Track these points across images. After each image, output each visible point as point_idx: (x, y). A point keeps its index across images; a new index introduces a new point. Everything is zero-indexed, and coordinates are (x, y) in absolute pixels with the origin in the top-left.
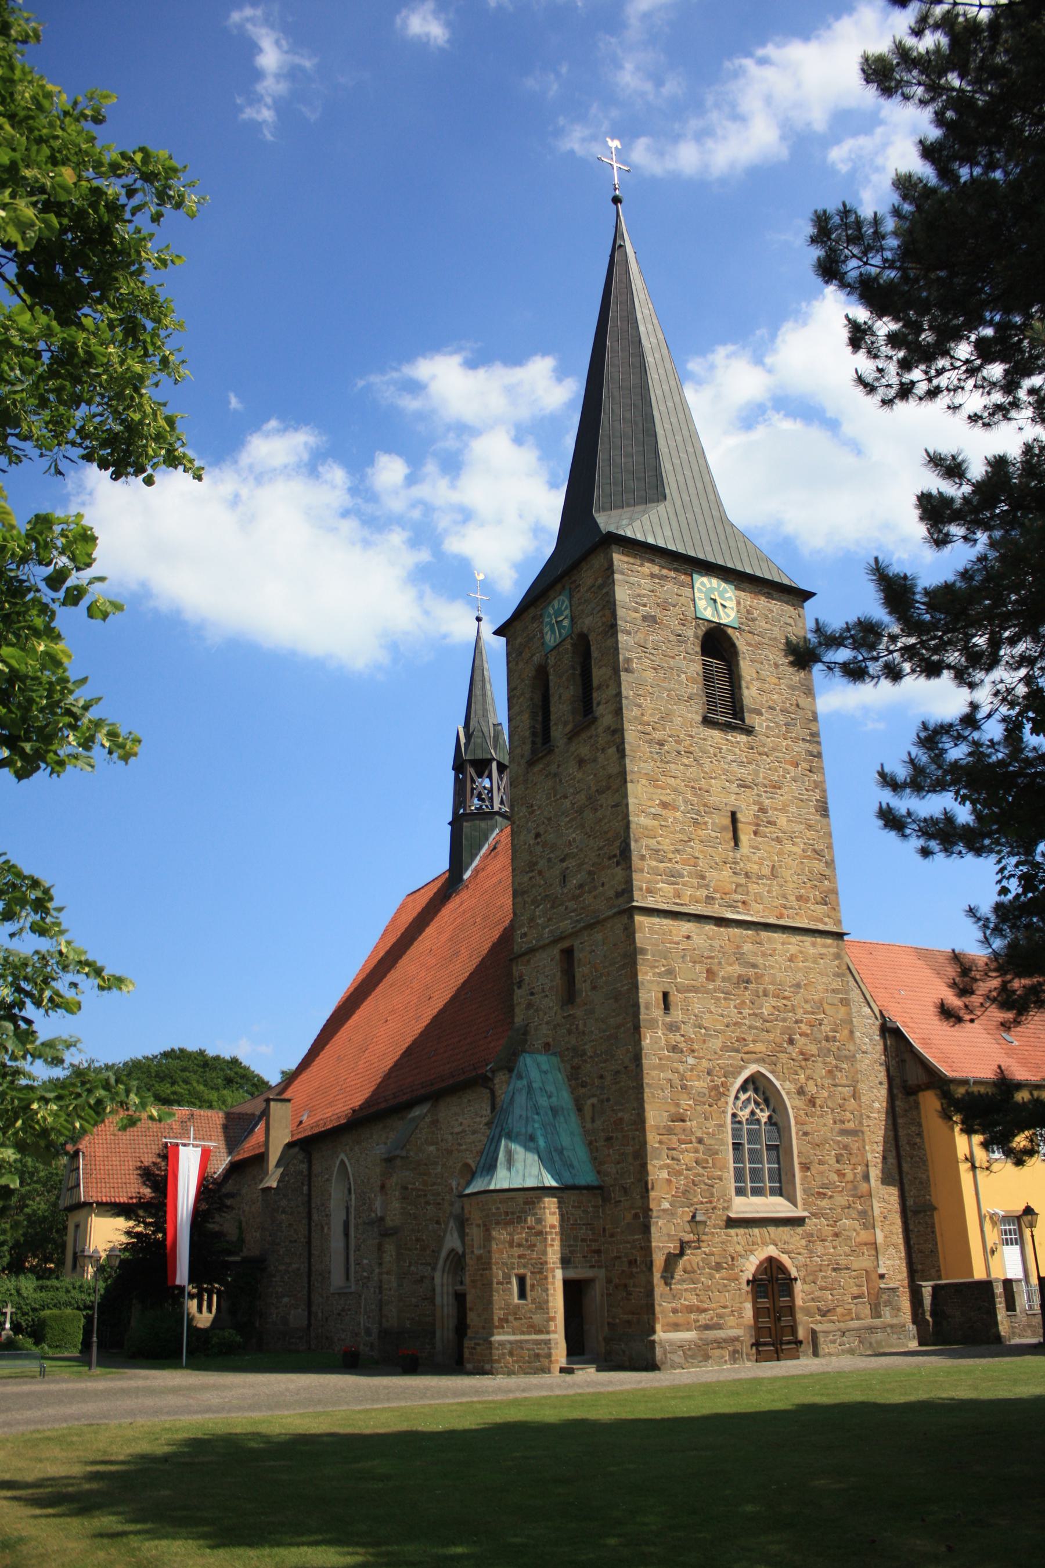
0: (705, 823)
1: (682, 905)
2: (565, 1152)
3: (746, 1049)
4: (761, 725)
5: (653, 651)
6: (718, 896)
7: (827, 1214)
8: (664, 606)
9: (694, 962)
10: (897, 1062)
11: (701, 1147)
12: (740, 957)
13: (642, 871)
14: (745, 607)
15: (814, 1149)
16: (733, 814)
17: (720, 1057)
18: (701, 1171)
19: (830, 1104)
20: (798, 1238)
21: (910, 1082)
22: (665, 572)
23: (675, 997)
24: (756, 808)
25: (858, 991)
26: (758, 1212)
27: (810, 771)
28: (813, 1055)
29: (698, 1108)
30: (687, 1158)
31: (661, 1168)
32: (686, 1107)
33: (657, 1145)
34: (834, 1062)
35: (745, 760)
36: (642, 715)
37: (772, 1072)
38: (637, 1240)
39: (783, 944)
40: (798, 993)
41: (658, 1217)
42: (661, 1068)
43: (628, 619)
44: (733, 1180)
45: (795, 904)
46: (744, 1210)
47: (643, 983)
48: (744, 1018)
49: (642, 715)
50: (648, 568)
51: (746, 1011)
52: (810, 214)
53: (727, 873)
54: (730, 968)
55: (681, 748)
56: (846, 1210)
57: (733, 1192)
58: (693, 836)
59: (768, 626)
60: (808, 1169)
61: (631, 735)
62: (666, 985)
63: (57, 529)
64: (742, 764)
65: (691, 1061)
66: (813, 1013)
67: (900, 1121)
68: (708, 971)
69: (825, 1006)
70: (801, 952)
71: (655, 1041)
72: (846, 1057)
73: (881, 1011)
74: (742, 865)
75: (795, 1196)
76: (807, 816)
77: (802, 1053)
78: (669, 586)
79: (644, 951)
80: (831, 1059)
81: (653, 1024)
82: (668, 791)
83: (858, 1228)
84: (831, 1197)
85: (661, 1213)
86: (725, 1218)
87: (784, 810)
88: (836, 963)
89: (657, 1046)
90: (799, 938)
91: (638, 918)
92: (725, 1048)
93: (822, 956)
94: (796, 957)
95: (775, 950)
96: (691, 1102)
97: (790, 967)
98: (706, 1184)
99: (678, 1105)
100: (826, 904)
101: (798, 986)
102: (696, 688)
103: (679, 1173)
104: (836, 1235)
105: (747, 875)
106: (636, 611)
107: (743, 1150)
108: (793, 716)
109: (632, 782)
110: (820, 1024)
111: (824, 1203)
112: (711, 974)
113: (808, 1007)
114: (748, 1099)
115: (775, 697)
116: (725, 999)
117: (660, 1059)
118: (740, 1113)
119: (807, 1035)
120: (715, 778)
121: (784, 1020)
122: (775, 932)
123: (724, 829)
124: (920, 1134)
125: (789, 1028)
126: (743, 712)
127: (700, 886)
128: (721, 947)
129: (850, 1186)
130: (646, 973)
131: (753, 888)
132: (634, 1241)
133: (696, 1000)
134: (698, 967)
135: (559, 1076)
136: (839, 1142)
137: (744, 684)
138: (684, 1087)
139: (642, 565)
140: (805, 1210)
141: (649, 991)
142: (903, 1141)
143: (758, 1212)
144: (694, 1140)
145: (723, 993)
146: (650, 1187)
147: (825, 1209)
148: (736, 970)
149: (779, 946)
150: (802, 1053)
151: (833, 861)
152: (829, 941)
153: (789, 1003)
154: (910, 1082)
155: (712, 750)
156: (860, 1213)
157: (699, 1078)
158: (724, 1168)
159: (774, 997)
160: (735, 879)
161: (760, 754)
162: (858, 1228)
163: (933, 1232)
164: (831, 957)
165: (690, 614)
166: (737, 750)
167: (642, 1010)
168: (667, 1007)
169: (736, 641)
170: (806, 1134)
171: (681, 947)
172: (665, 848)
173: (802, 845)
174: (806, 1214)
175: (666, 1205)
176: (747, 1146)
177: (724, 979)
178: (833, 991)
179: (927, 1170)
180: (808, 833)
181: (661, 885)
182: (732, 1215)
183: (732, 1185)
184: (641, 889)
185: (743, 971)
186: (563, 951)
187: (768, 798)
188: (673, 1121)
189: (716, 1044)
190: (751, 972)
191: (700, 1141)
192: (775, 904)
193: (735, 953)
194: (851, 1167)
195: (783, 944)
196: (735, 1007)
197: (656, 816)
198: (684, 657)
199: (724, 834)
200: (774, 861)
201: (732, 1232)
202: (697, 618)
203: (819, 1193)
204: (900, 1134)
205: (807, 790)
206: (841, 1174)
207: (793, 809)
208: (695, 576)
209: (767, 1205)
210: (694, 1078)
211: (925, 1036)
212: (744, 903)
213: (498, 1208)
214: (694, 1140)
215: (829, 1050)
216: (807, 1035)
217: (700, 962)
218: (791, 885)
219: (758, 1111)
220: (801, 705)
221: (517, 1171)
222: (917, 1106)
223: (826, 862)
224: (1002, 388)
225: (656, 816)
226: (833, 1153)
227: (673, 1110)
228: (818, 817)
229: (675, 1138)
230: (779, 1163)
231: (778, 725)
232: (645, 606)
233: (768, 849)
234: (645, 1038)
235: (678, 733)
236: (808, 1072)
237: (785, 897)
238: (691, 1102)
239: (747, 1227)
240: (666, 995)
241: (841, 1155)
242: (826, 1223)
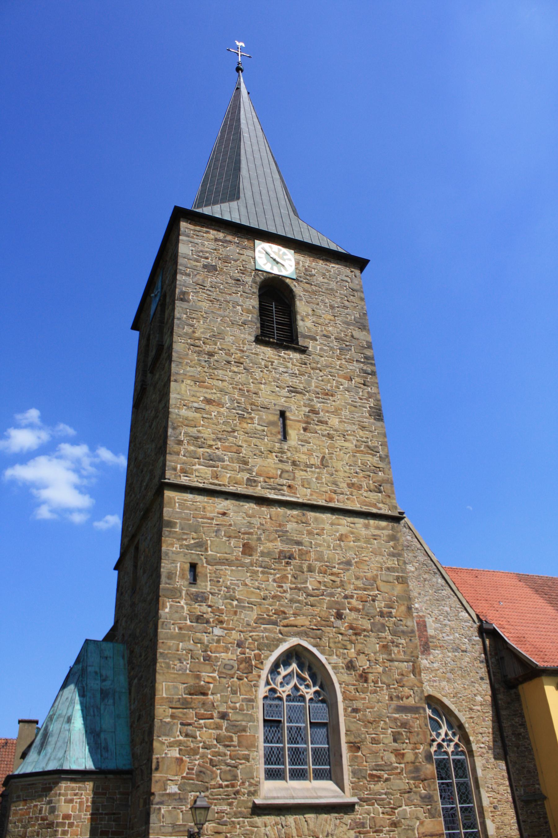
0: (252, 419)
1: (220, 485)
2: (102, 736)
3: (285, 622)
4: (315, 348)
5: (210, 289)
6: (261, 479)
7: (383, 800)
8: (226, 260)
9: (229, 537)
10: (497, 660)
11: (225, 724)
12: (283, 535)
13: (178, 454)
14: (303, 266)
15: (365, 726)
16: (283, 414)
17: (254, 630)
18: (222, 749)
19: (385, 679)
20: (345, 828)
21: (509, 677)
22: (229, 238)
23: (205, 569)
24: (307, 409)
25: (455, 598)
26: (293, 798)
27: (364, 385)
28: (364, 630)
29: (224, 681)
30: (205, 735)
31: (171, 745)
32: (207, 680)
33: (168, 720)
34: (390, 637)
35: (297, 372)
36: (194, 332)
37: (315, 646)
39: (332, 524)
40: (348, 570)
41: (162, 803)
42: (181, 638)
43: (189, 266)
44: (262, 760)
45: (346, 490)
46: (275, 795)
47: (167, 554)
48: (285, 592)
49: (194, 332)
50: (213, 233)
51: (287, 586)
53: (272, 461)
54: (270, 545)
55: (231, 359)
56: (406, 795)
57: (262, 775)
58: (238, 428)
59: (326, 281)
60: (359, 748)
61: (179, 346)
62: (194, 556)
63: (497, 657)
64: (294, 375)
65: (217, 631)
66: (365, 590)
67: (503, 713)
68: (244, 545)
69: (379, 582)
70: (352, 533)
71: (177, 610)
72: (403, 632)
73: (478, 616)
74: (289, 454)
75: (342, 779)
76: (361, 419)
77: (351, 628)
78: (231, 248)
79: (171, 524)
80: (387, 635)
81: (175, 594)
82: (214, 391)
83: (422, 816)
84: (387, 780)
85: (165, 798)
86: (250, 804)
87: (336, 412)
88: (392, 543)
89: (177, 615)
90: (350, 519)
91: (168, 494)
92: (260, 620)
93: (375, 537)
94: (346, 537)
95: (323, 529)
96: (215, 675)
97: (340, 546)
98: (228, 765)
99: (198, 677)
100: (380, 492)
101: (348, 563)
102: (253, 317)
103: (195, 752)
104: (394, 824)
105: (294, 463)
106: (197, 261)
107: (283, 729)
108: (348, 343)
109: (176, 381)
110: (374, 600)
111: (379, 787)
112: (248, 549)
113: (359, 583)
114: (290, 675)
115: (330, 329)
116: (263, 573)
117: (180, 629)
118: (280, 689)
119: (358, 610)
120: (265, 384)
121: (332, 595)
122: (323, 513)
123: (271, 424)
124: (523, 725)
125: (337, 603)
126: (297, 337)
127: (241, 470)
128: (261, 524)
129: (410, 767)
130: (172, 545)
131: (299, 474)
133: (229, 572)
134: (233, 542)
135: (121, 662)
136: (396, 719)
137: (299, 317)
138: (207, 659)
139: (207, 232)
140: (354, 795)
141: (174, 562)
142: (508, 732)
143: (293, 798)
144: (215, 715)
145: (261, 567)
146: (154, 766)
147: (381, 794)
148: (279, 546)
149: (327, 527)
150: (351, 628)
151: (387, 456)
152: (383, 524)
153: (338, 580)
154: (509, 677)
155: (263, 363)
156: (423, 798)
157: (226, 650)
158: (252, 746)
159: (320, 572)
160: (281, 466)
161: (312, 369)
162: (422, 816)
163: (547, 823)
164: (385, 538)
165: (250, 266)
166: (290, 365)
167: (163, 579)
168: (194, 581)
169: (293, 288)
170: (356, 710)
171: (214, 522)
172: (205, 436)
173: (355, 442)
174: (355, 800)
175: (173, 789)
176: (286, 724)
177: (263, 554)
178: (388, 569)
179: (533, 759)
180: (361, 433)
181: (197, 467)
182: (258, 801)
183: (261, 767)
184: (175, 469)
185: (286, 548)
187: (320, 403)
188: (191, 694)
189: (252, 616)
190: (295, 549)
191: (224, 716)
192: (324, 489)
193: (277, 531)
194: (411, 746)
195: (332, 524)
196: (274, 581)
197: (197, 409)
198: (241, 295)
199: (271, 427)
200: (325, 453)
201: (258, 820)
202: (256, 270)
203: (371, 776)
204: (504, 725)
205: (361, 399)
206: (400, 755)
207: (345, 413)
208: (257, 242)
209: (308, 790)
210: (221, 650)
211: (520, 635)
212: (289, 486)
214: (215, 715)
215: (383, 625)
216: (358, 610)
217: (236, 537)
218: (341, 474)
219: (302, 687)
220: (355, 336)
221: (46, 755)
222: (518, 698)
223: (380, 457)
225: (197, 409)
226: (389, 731)
227: (192, 682)
228: (372, 421)
229: (192, 713)
230: (328, 744)
231: (332, 349)
232: (207, 258)
233: (317, 442)
234: (164, 607)
235: (229, 348)
236: (359, 646)
237: (335, 483)
238: (215, 675)
239: (278, 815)
240: (193, 567)
241: (399, 733)
242: (381, 810)
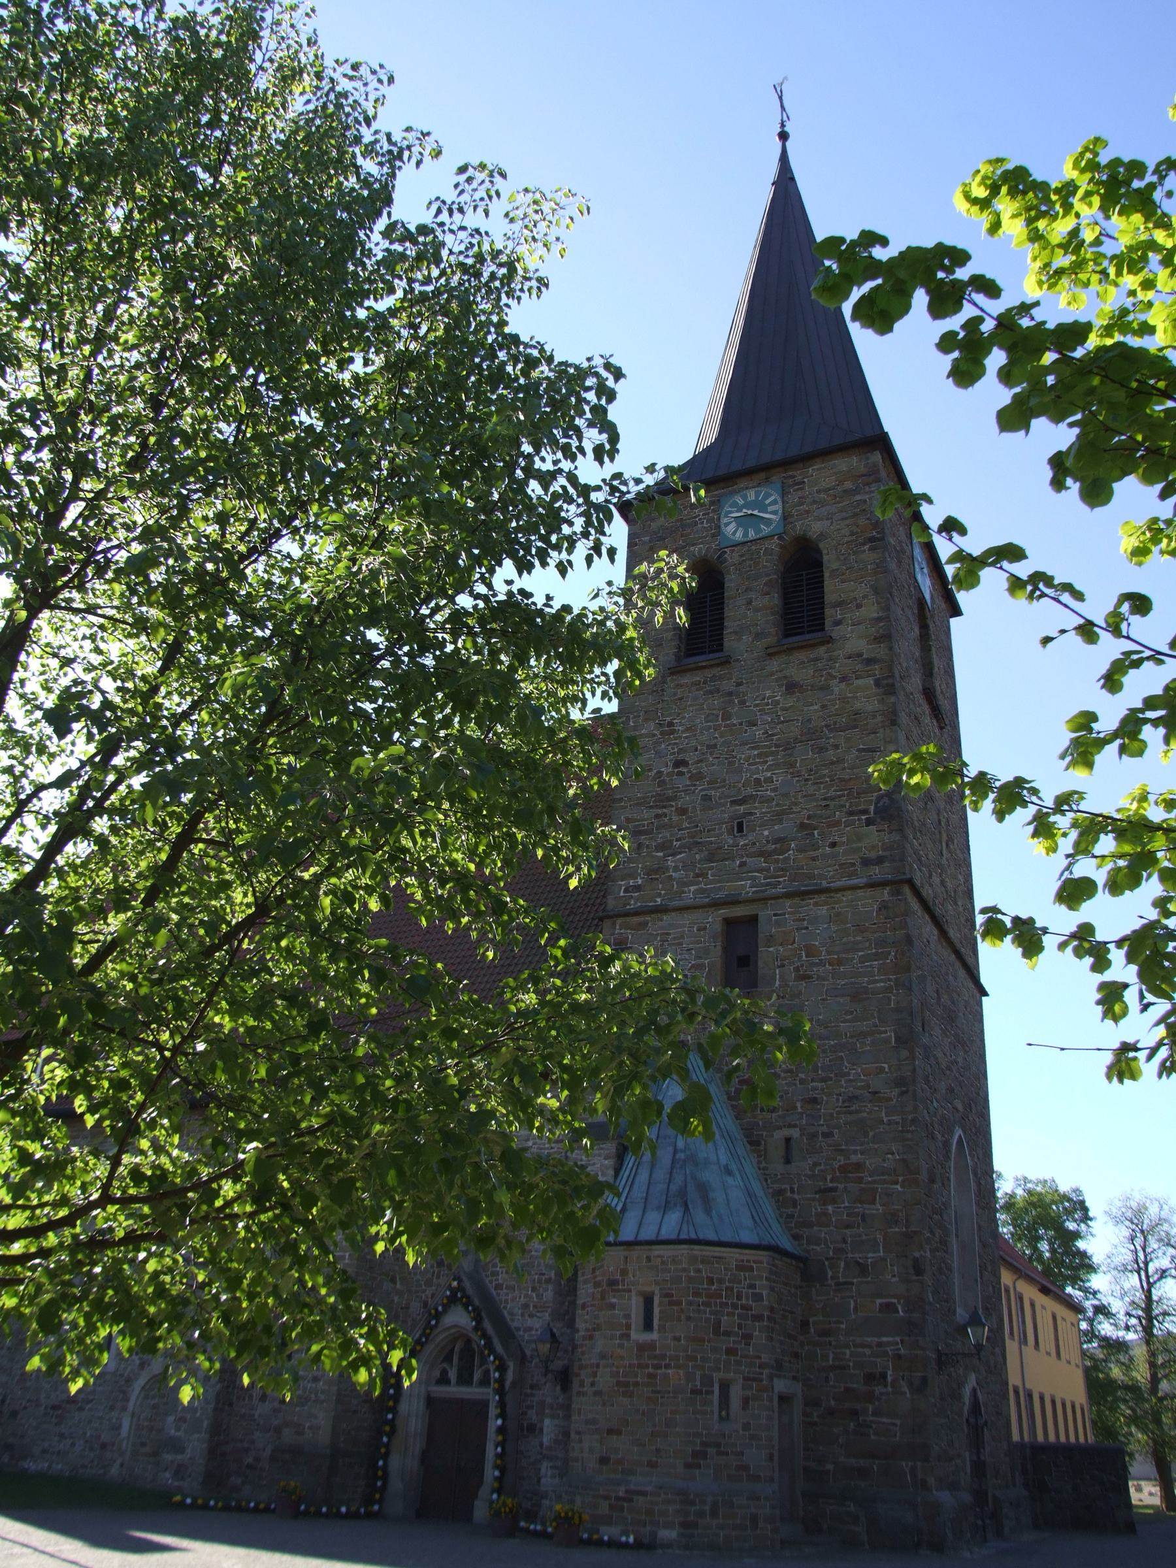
38: (888, 1344)
52: (996, 237)
132: (880, 1344)
186: (728, 922)
213: (699, 1271)
224: (647, 633)
